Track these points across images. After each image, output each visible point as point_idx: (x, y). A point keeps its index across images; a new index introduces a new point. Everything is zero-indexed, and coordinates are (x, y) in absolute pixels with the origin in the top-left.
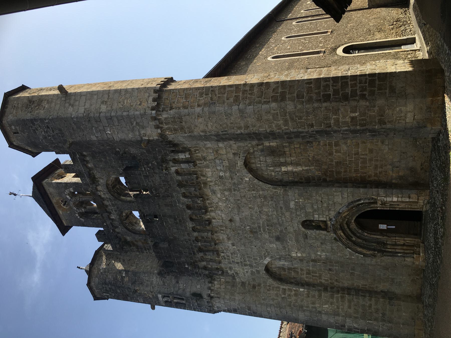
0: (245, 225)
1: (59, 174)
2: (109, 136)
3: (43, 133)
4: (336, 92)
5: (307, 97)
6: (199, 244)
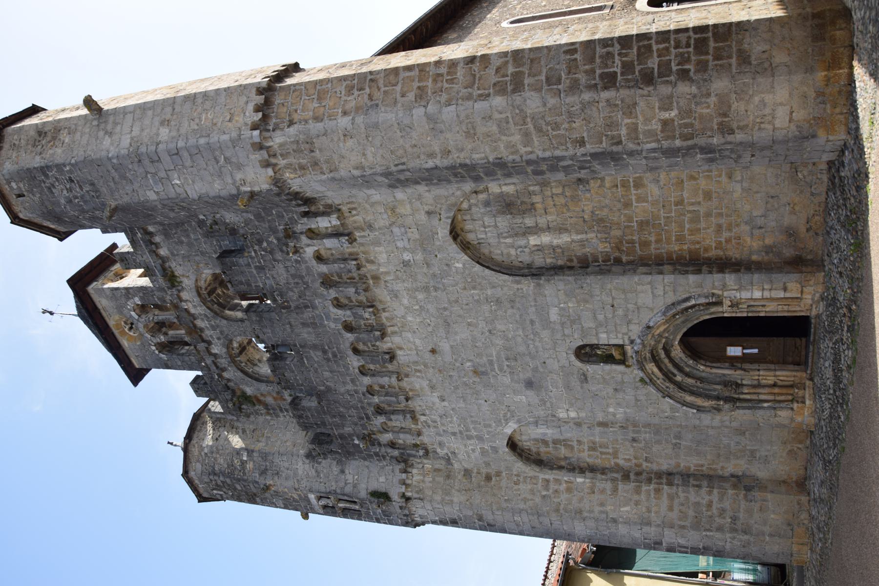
1: (117, 273)
2: (179, 190)
3: (65, 192)
4: (628, 67)
5: (568, 81)
6: (376, 400)
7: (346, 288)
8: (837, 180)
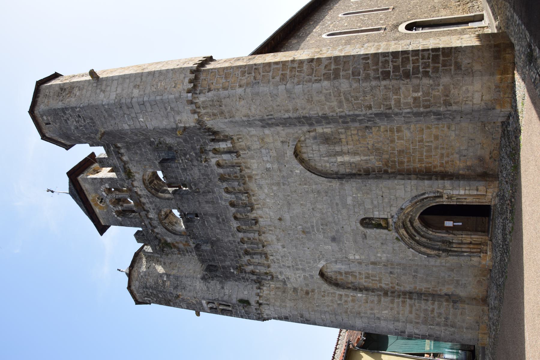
0: (297, 224)
1: (94, 169)
2: (142, 124)
3: (75, 123)
4: (396, 68)
5: (364, 75)
6: (245, 246)
7: (233, 182)
8: (506, 132)
